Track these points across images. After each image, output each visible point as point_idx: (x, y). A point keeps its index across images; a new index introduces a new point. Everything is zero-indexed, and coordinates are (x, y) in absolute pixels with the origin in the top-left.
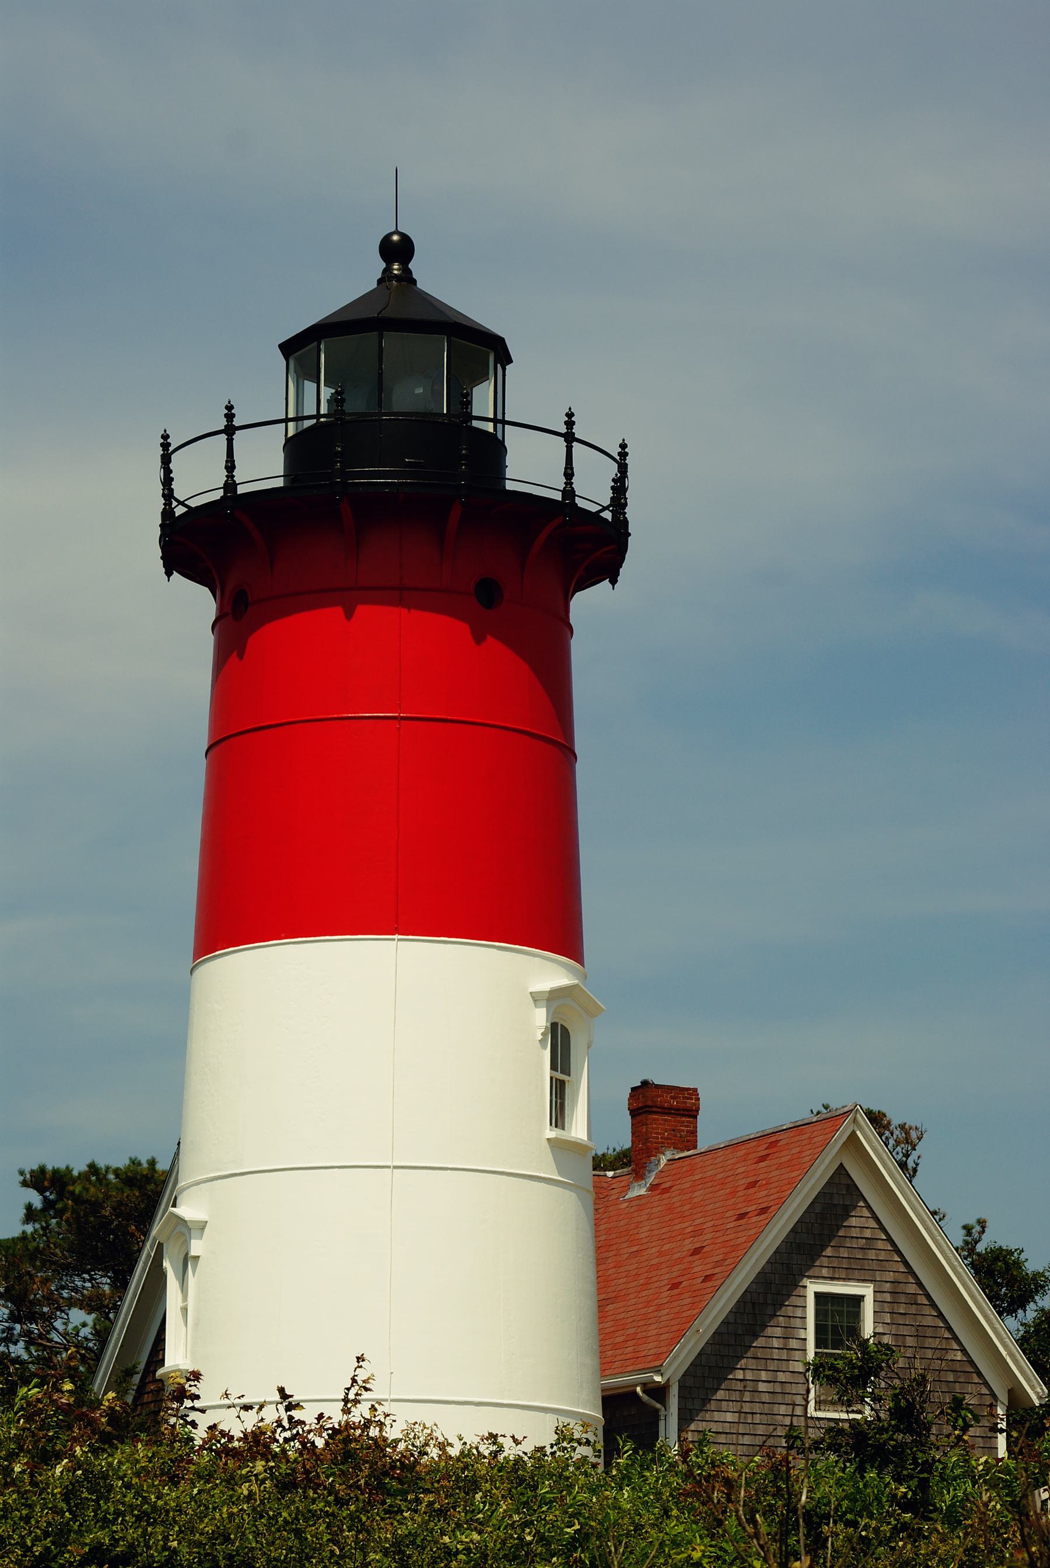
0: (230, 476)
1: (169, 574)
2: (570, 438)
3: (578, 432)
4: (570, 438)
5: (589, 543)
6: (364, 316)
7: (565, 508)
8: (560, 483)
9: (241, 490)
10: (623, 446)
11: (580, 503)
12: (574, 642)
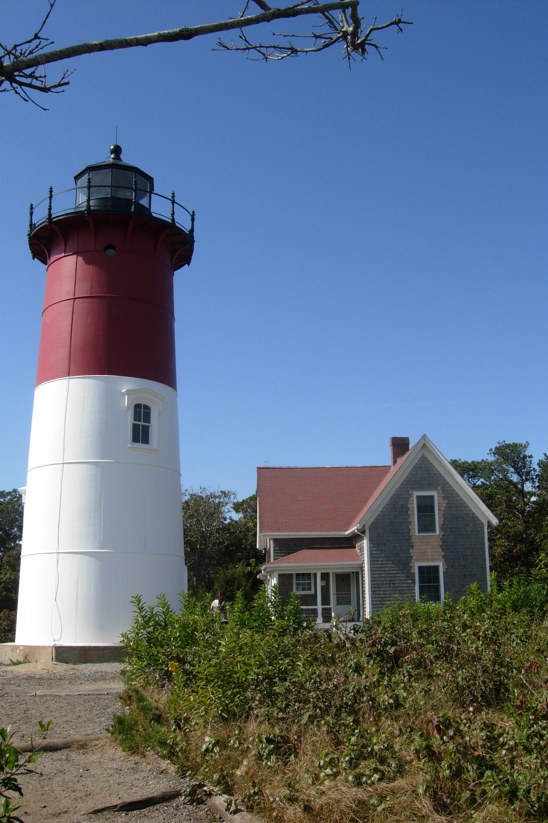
0: (50, 212)
1: (34, 258)
2: (173, 202)
4: (173, 202)
6: (179, 428)
7: (170, 228)
8: (170, 216)
12: (174, 277)
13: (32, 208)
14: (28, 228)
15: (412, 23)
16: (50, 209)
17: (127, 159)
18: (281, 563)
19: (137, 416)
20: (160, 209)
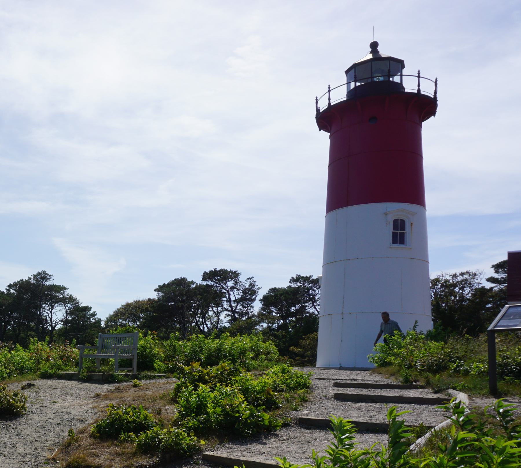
1: (320, 130)
2: (419, 77)
3: (421, 75)
4: (419, 77)
5: (426, 106)
7: (418, 96)
8: (417, 88)
9: (332, 104)
10: (436, 79)
11: (422, 93)
13: (317, 100)
14: (315, 113)
15: (416, 322)
16: (329, 99)
17: (384, 51)
18: (255, 453)
19: (395, 227)
20: (410, 86)
